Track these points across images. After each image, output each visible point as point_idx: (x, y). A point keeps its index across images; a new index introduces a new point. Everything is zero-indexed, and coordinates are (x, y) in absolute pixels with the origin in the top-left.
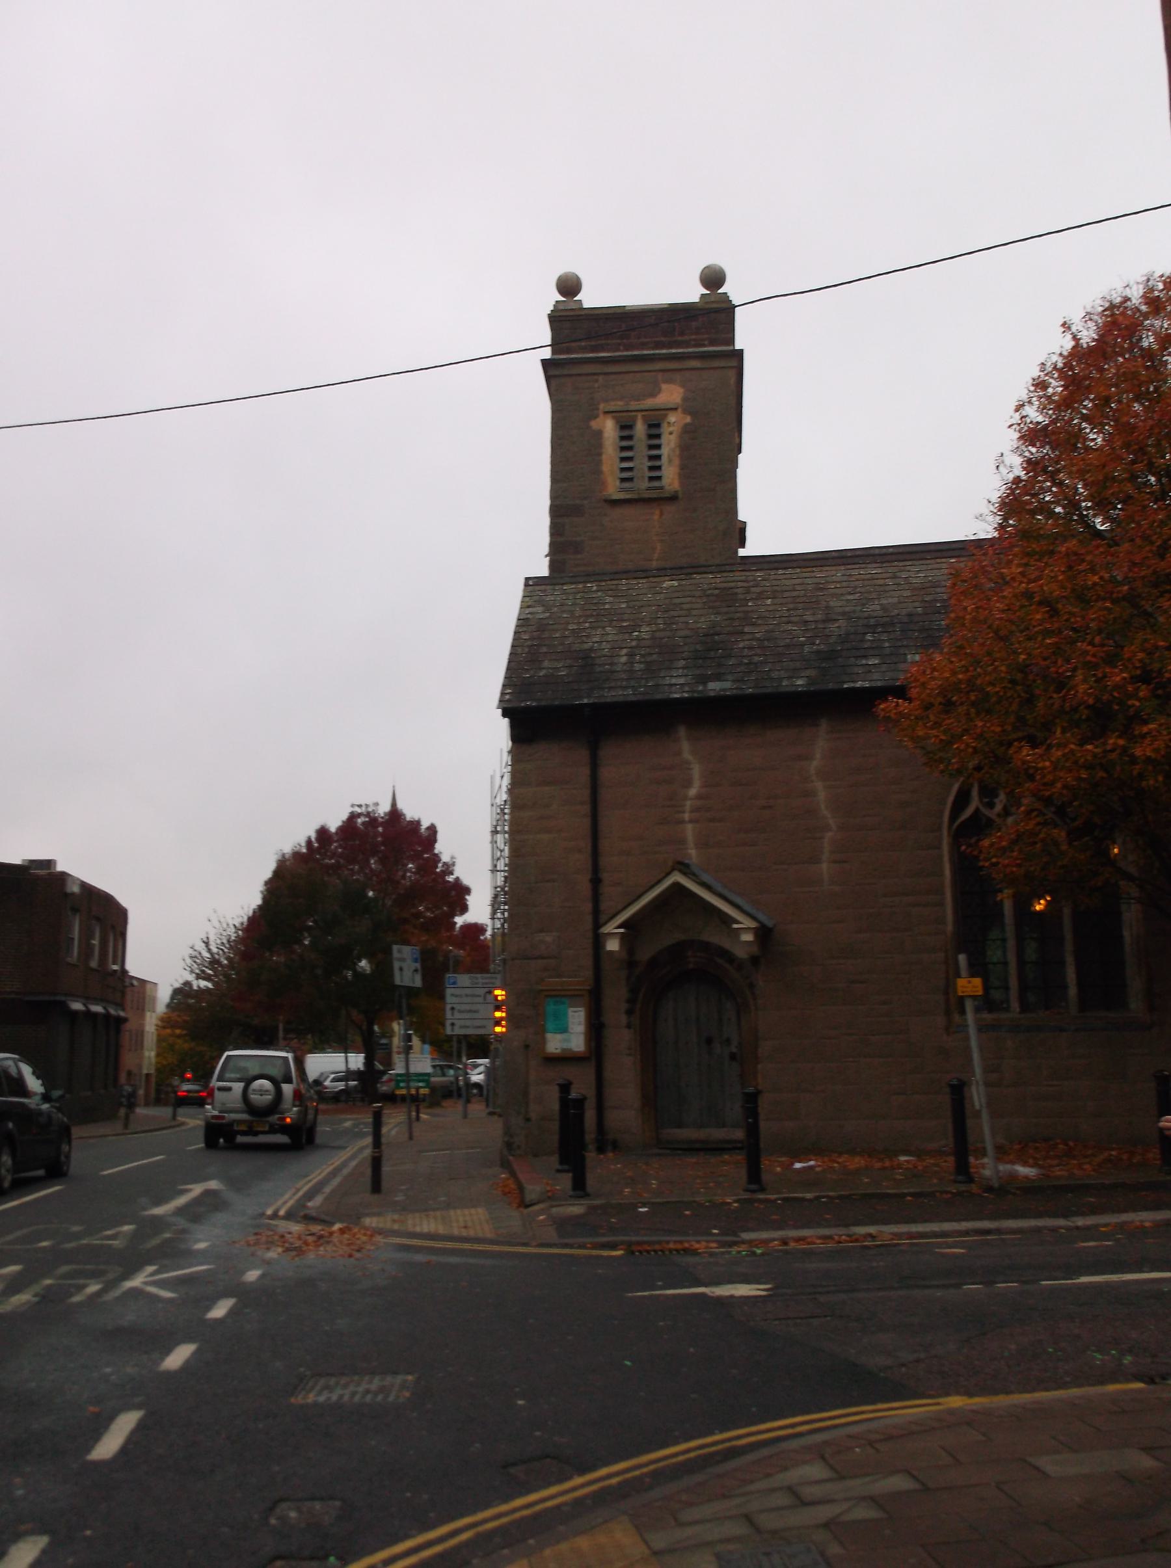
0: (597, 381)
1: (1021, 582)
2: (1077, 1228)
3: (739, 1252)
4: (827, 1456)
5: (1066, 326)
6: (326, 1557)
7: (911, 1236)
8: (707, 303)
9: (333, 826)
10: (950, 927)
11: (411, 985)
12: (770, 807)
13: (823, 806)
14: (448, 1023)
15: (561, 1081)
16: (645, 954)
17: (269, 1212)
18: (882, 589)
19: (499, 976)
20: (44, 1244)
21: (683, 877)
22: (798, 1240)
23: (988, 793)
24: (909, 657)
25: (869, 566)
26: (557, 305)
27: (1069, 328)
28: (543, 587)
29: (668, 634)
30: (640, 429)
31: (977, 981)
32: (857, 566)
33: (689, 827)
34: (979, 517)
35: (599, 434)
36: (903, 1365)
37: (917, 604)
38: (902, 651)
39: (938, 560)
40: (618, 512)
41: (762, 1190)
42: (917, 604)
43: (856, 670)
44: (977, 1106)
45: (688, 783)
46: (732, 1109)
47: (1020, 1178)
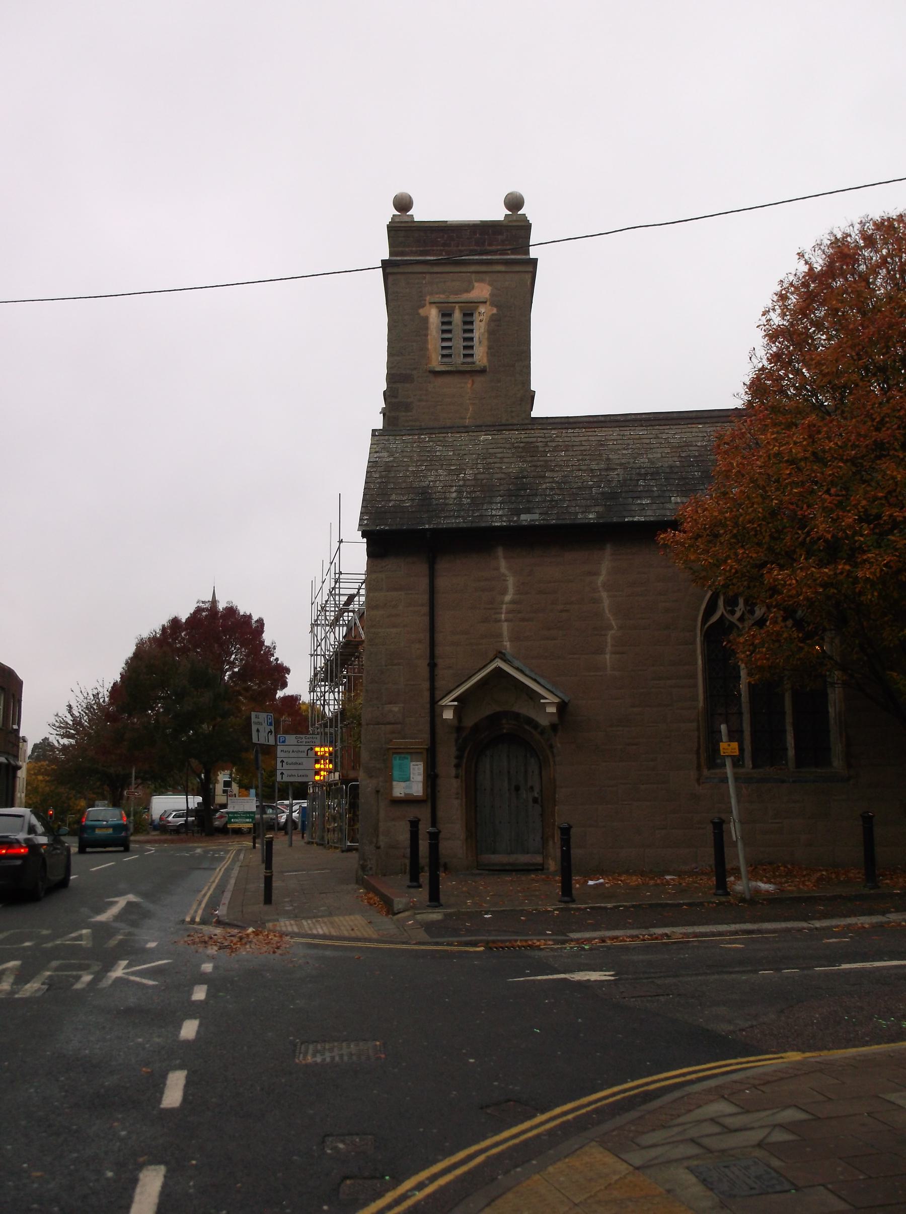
0: (425, 278)
2: (816, 928)
3: (572, 948)
4: (726, 1096)
5: (801, 255)
6: (383, 1177)
7: (696, 935)
9: (184, 617)
10: (701, 704)
11: (267, 743)
12: (567, 611)
13: (607, 612)
14: (279, 772)
15: (411, 818)
16: (469, 722)
17: (188, 919)
18: (648, 446)
19: (318, 737)
20: (27, 944)
21: (504, 663)
23: (731, 603)
24: (673, 498)
25: (637, 428)
26: (395, 218)
27: (803, 256)
28: (387, 437)
29: (487, 476)
30: (457, 316)
31: (735, 745)
32: (628, 429)
35: (426, 320)
36: (743, 1030)
38: (667, 494)
39: (689, 426)
40: (440, 381)
41: (573, 901)
42: (676, 459)
44: (734, 839)
45: (504, 592)
46: (534, 840)
47: (763, 892)
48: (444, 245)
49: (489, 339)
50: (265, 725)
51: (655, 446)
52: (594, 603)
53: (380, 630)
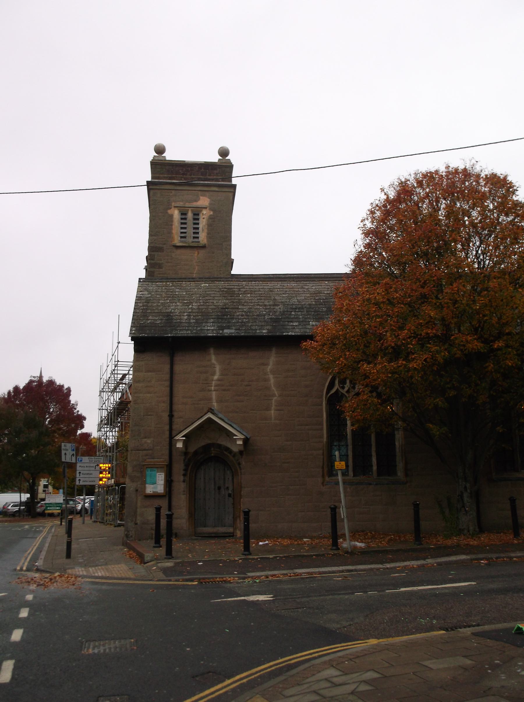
1: (367, 295)
2: (387, 568)
3: (249, 582)
4: (334, 665)
5: (382, 190)
7: (320, 573)
8: (221, 163)
9: (21, 386)
10: (325, 440)
12: (250, 385)
13: (272, 386)
14: (77, 479)
15: (156, 506)
16: (192, 449)
17: (18, 568)
18: (297, 293)
22: (273, 576)
23: (343, 382)
25: (291, 282)
27: (383, 190)
28: (147, 283)
29: (205, 307)
30: (190, 215)
31: (343, 463)
33: (214, 393)
34: (346, 265)
35: (171, 216)
36: (345, 627)
37: (313, 300)
40: (179, 251)
41: (250, 554)
43: (288, 327)
45: (214, 374)
48: (183, 174)
49: (208, 229)
50: (70, 450)
51: (301, 292)
52: (265, 381)
53: (141, 395)
